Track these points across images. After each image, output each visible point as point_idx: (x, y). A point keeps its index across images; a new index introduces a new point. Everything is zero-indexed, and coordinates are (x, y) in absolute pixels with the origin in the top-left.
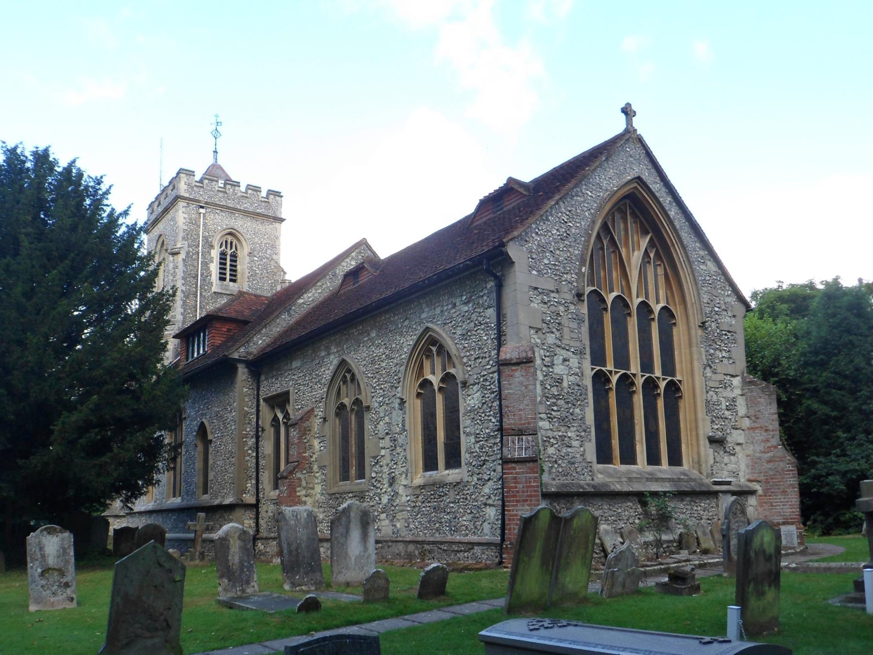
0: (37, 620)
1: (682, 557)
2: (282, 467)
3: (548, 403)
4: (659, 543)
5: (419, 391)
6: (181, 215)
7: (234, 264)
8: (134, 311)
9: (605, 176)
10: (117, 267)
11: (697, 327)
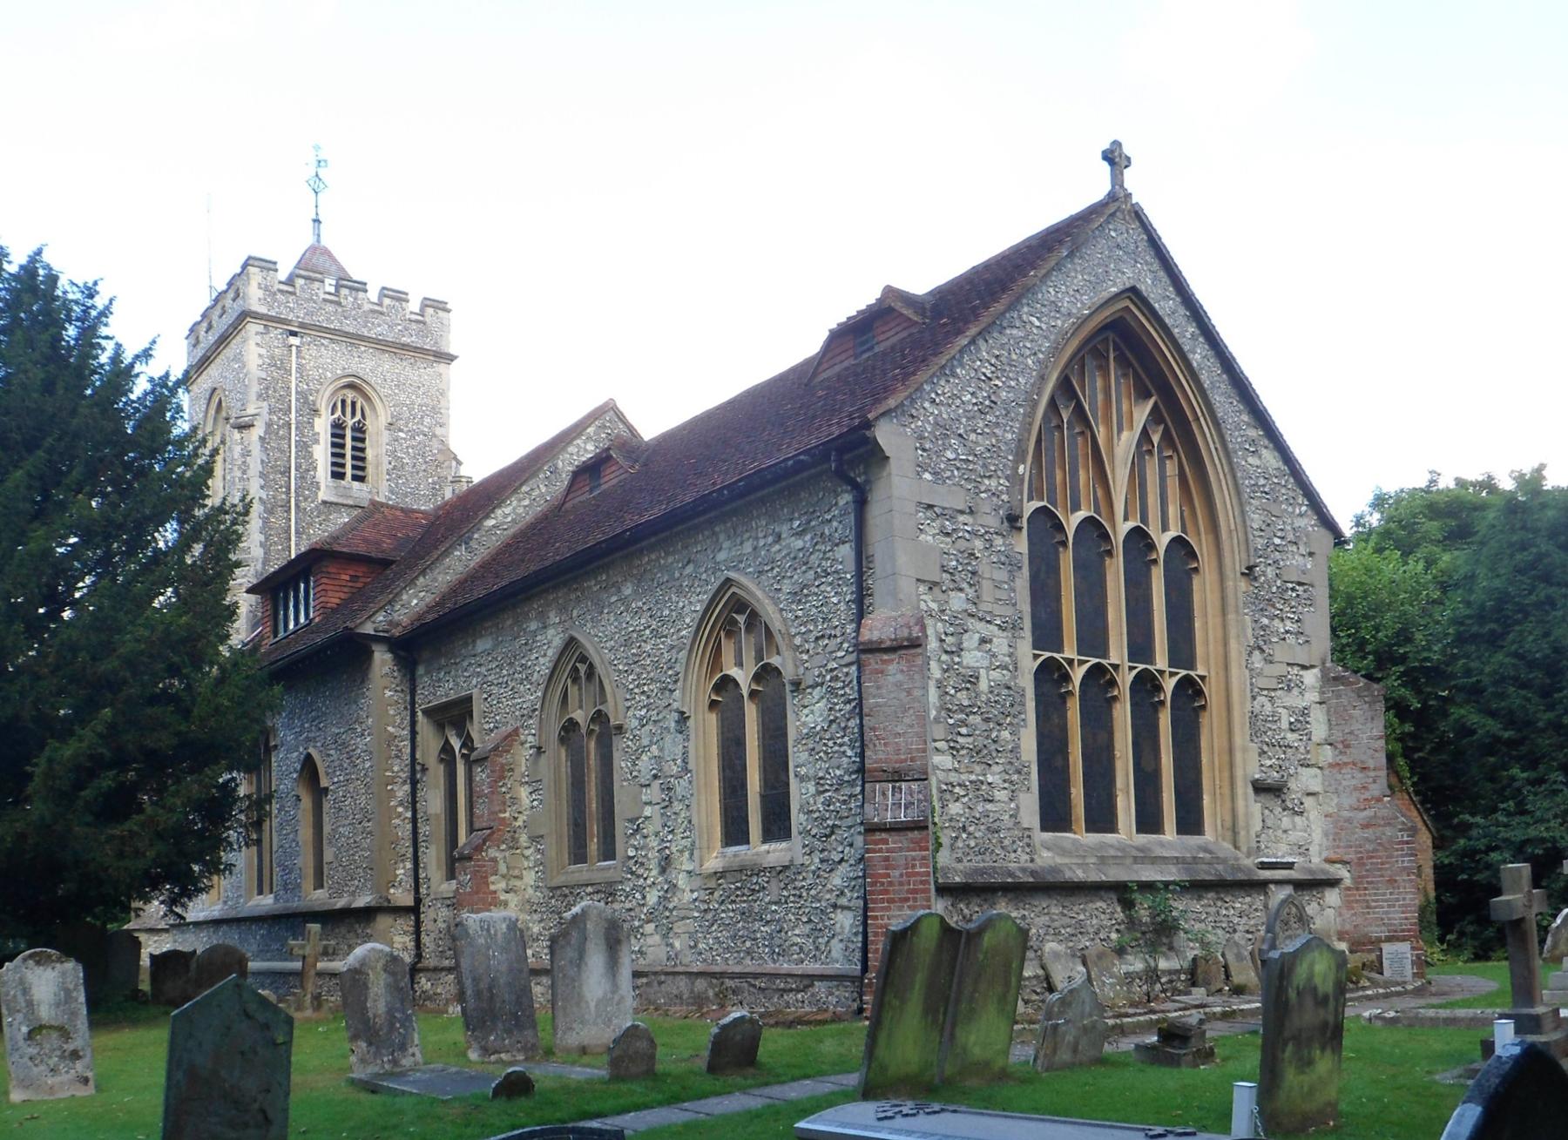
0: (29, 1117)
1: (1193, 1000)
2: (462, 838)
4: (1152, 975)
5: (714, 697)
6: (253, 348)
7: (360, 445)
8: (170, 544)
9: (1067, 287)
10: (135, 459)
11: (1238, 574)
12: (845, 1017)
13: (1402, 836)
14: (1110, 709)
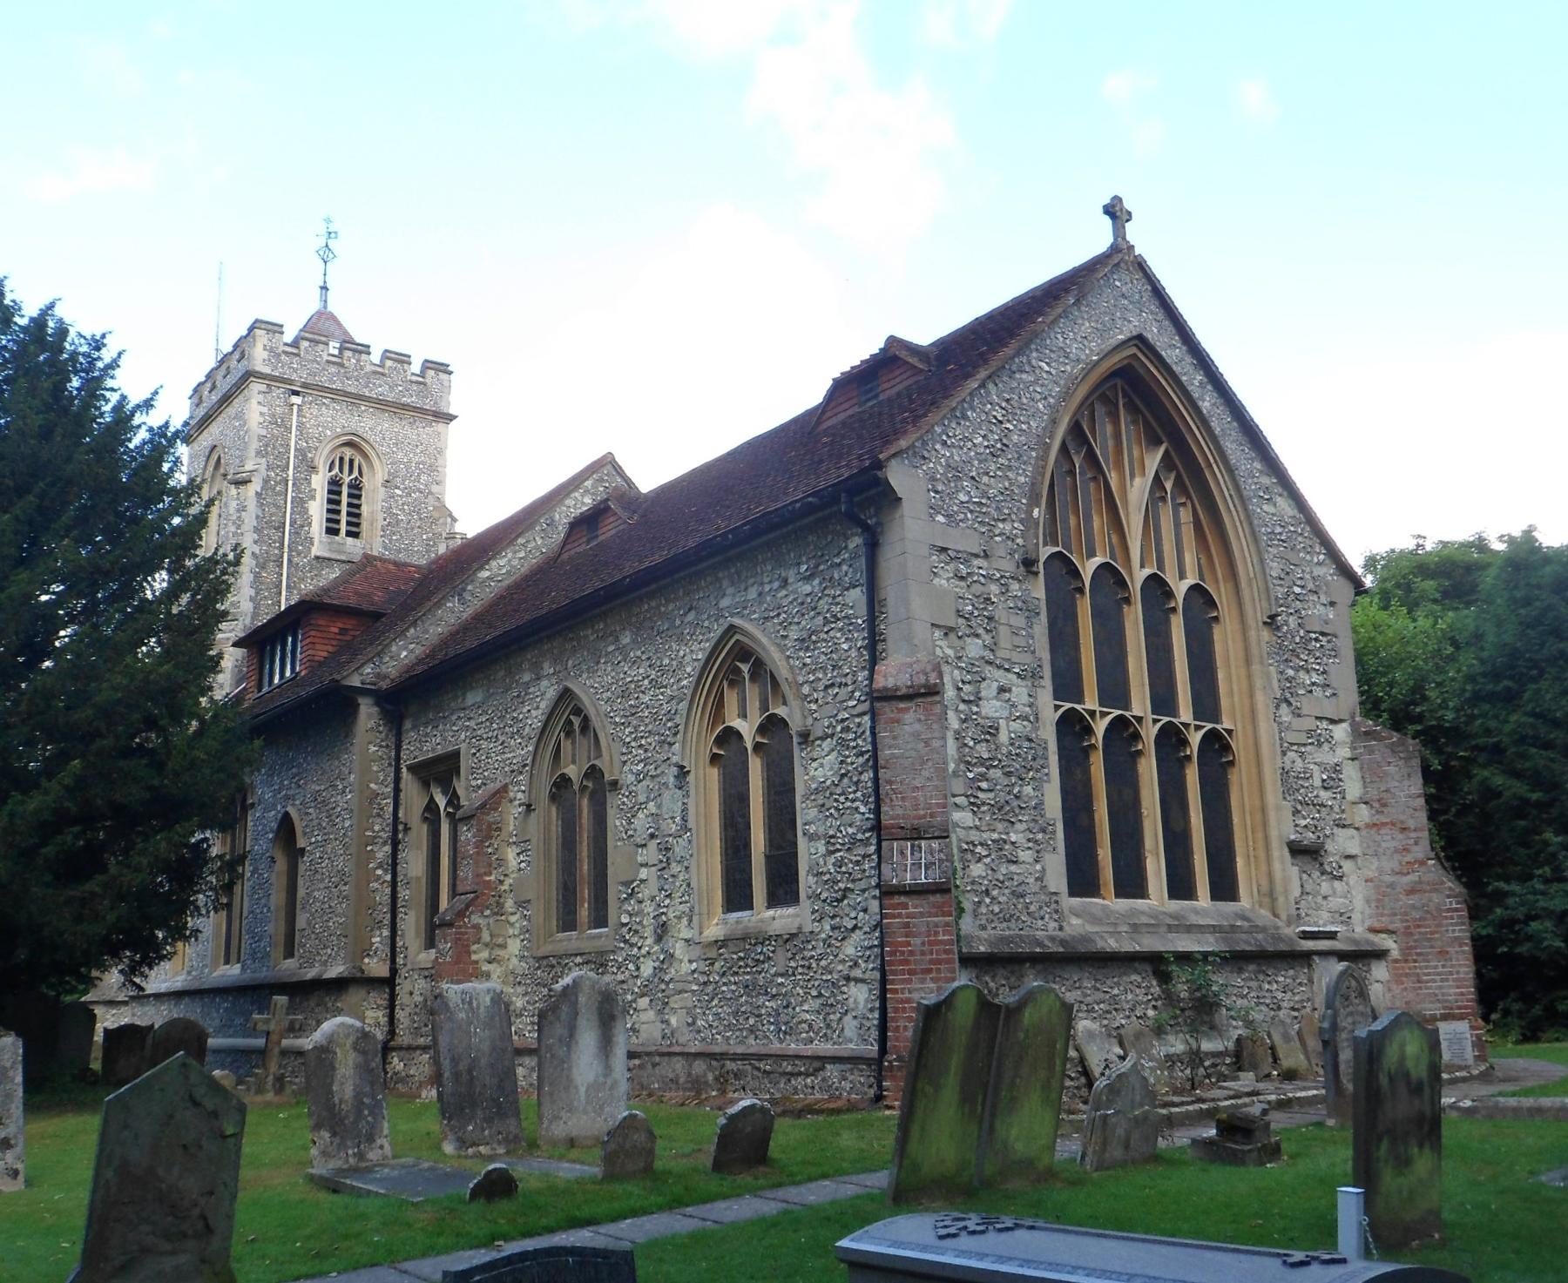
1: (1242, 1086)
2: (444, 904)
3: (971, 775)
4: (1195, 1057)
5: (715, 751)
6: (255, 408)
7: (355, 501)
9: (1074, 333)
10: (127, 509)
11: (1261, 624)
12: (861, 1107)
13: (1451, 902)
14: (1134, 764)
